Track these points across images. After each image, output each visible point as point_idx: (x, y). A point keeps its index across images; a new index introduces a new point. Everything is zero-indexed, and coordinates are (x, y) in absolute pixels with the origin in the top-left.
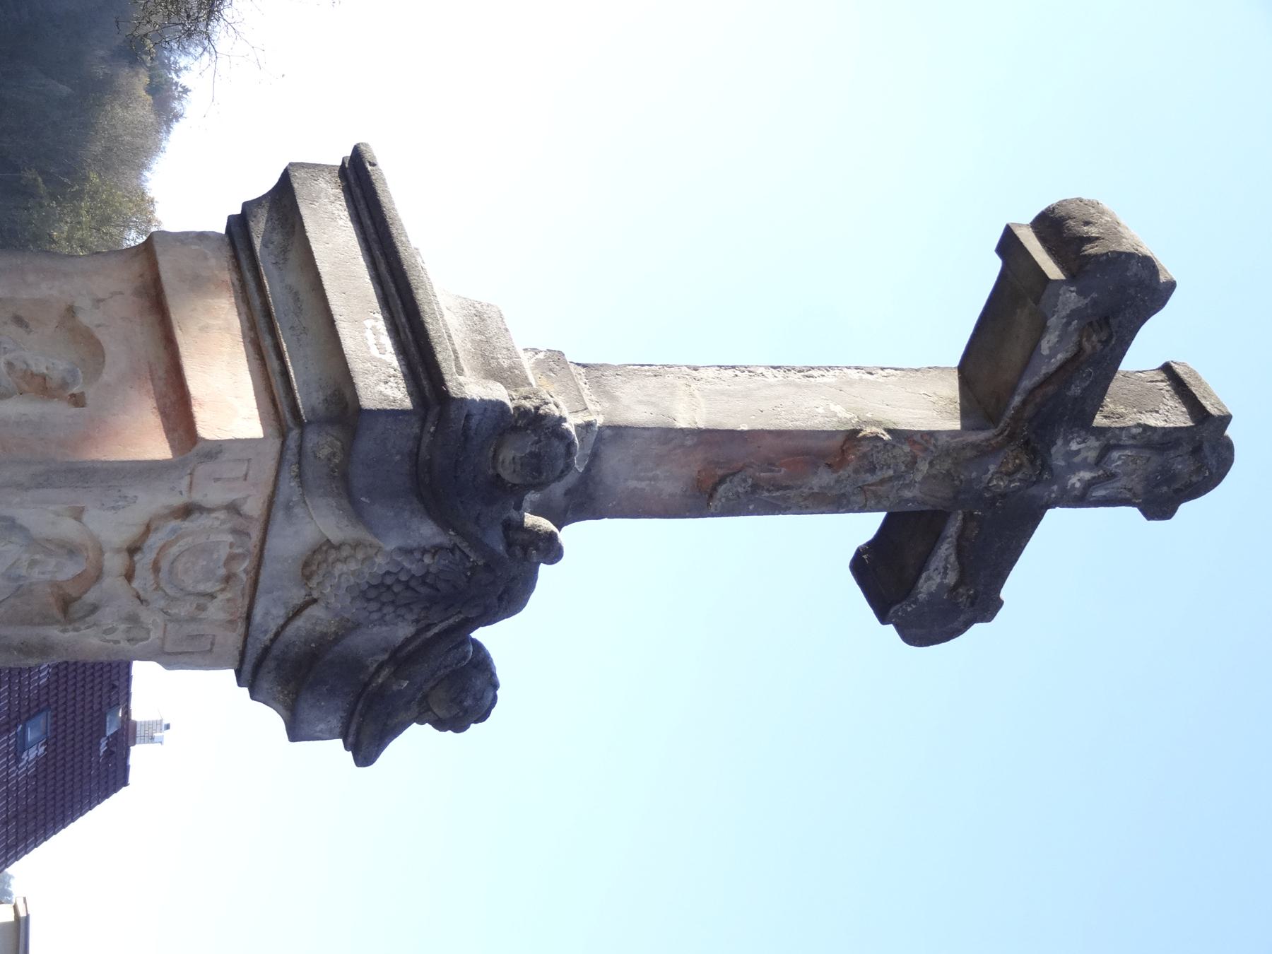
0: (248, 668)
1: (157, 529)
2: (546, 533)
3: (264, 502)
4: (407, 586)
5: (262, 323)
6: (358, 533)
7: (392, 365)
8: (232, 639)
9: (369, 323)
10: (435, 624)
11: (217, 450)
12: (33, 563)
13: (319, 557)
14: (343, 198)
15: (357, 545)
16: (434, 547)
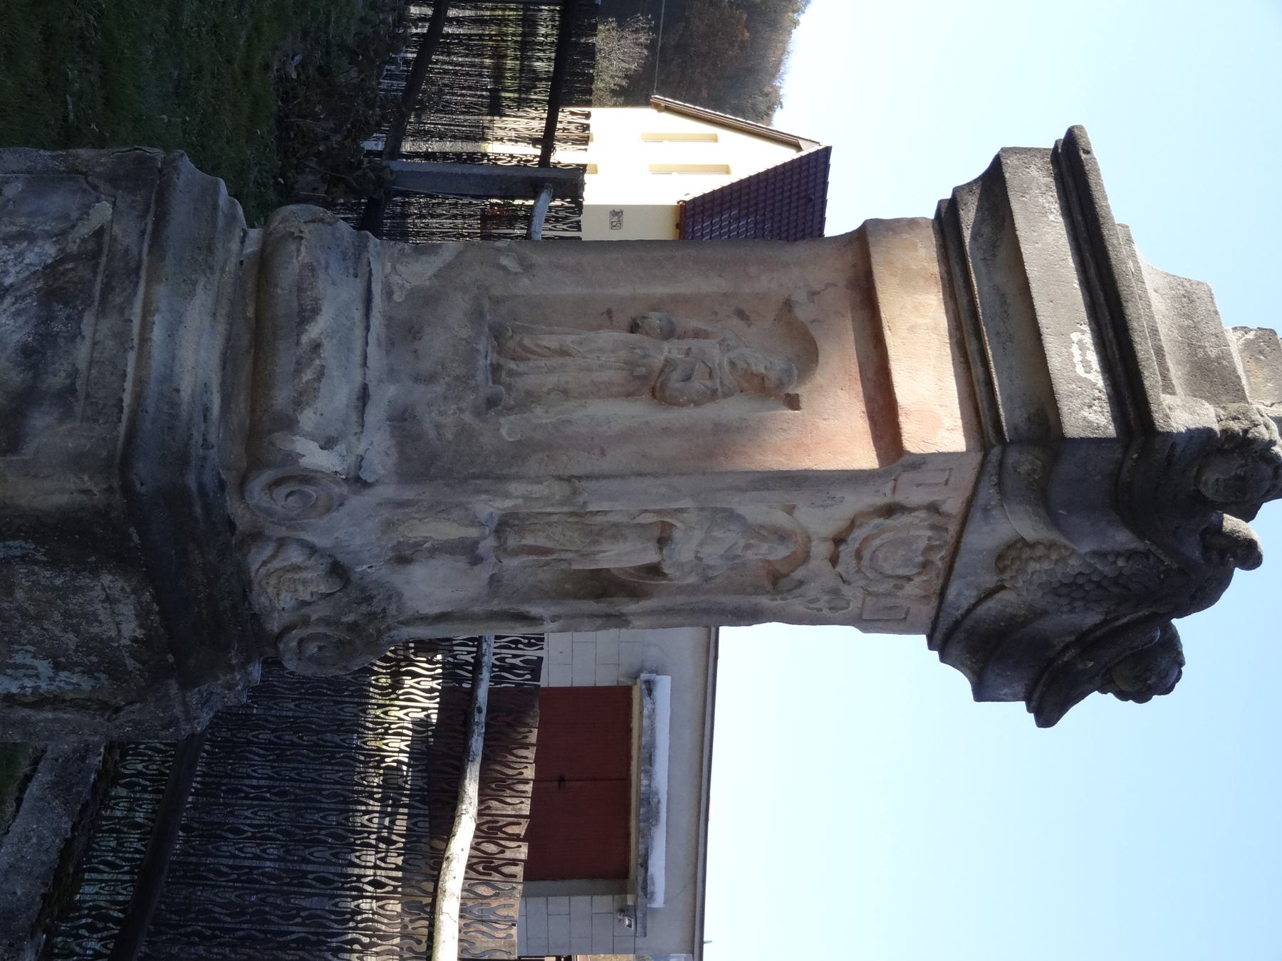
0: (939, 636)
1: (861, 526)
2: (1246, 539)
3: (963, 502)
4: (1099, 585)
5: (967, 327)
6: (1053, 535)
7: (1098, 385)
8: (926, 611)
9: (1075, 336)
10: (1125, 616)
11: (920, 462)
12: (747, 547)
13: (1013, 553)
14: (1054, 188)
15: (1051, 546)
16: (1127, 551)
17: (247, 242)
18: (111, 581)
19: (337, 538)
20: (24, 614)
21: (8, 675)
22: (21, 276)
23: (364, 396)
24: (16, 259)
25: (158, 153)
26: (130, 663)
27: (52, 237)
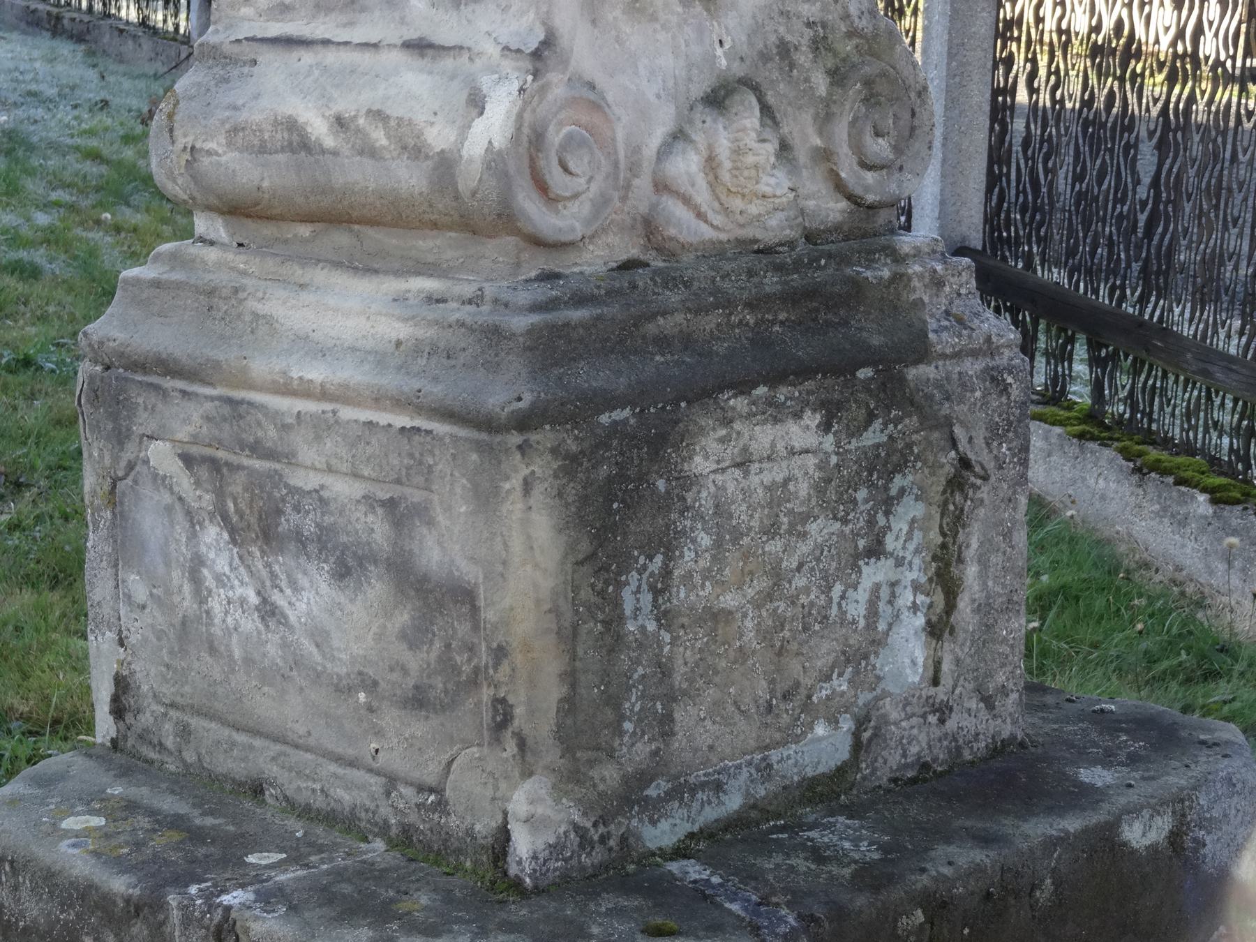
17: (212, 236)
18: (706, 458)
19: (658, 96)
20: (770, 597)
21: (890, 629)
22: (247, 579)
23: (420, 47)
24: (224, 586)
25: (85, 369)
26: (873, 436)
27: (195, 531)
